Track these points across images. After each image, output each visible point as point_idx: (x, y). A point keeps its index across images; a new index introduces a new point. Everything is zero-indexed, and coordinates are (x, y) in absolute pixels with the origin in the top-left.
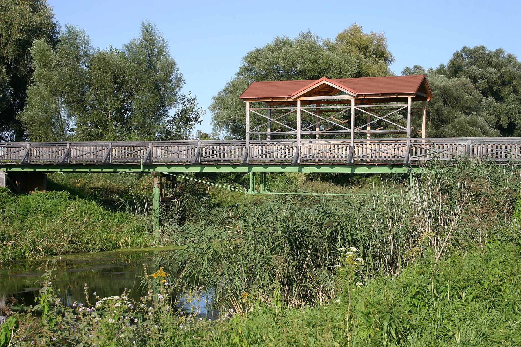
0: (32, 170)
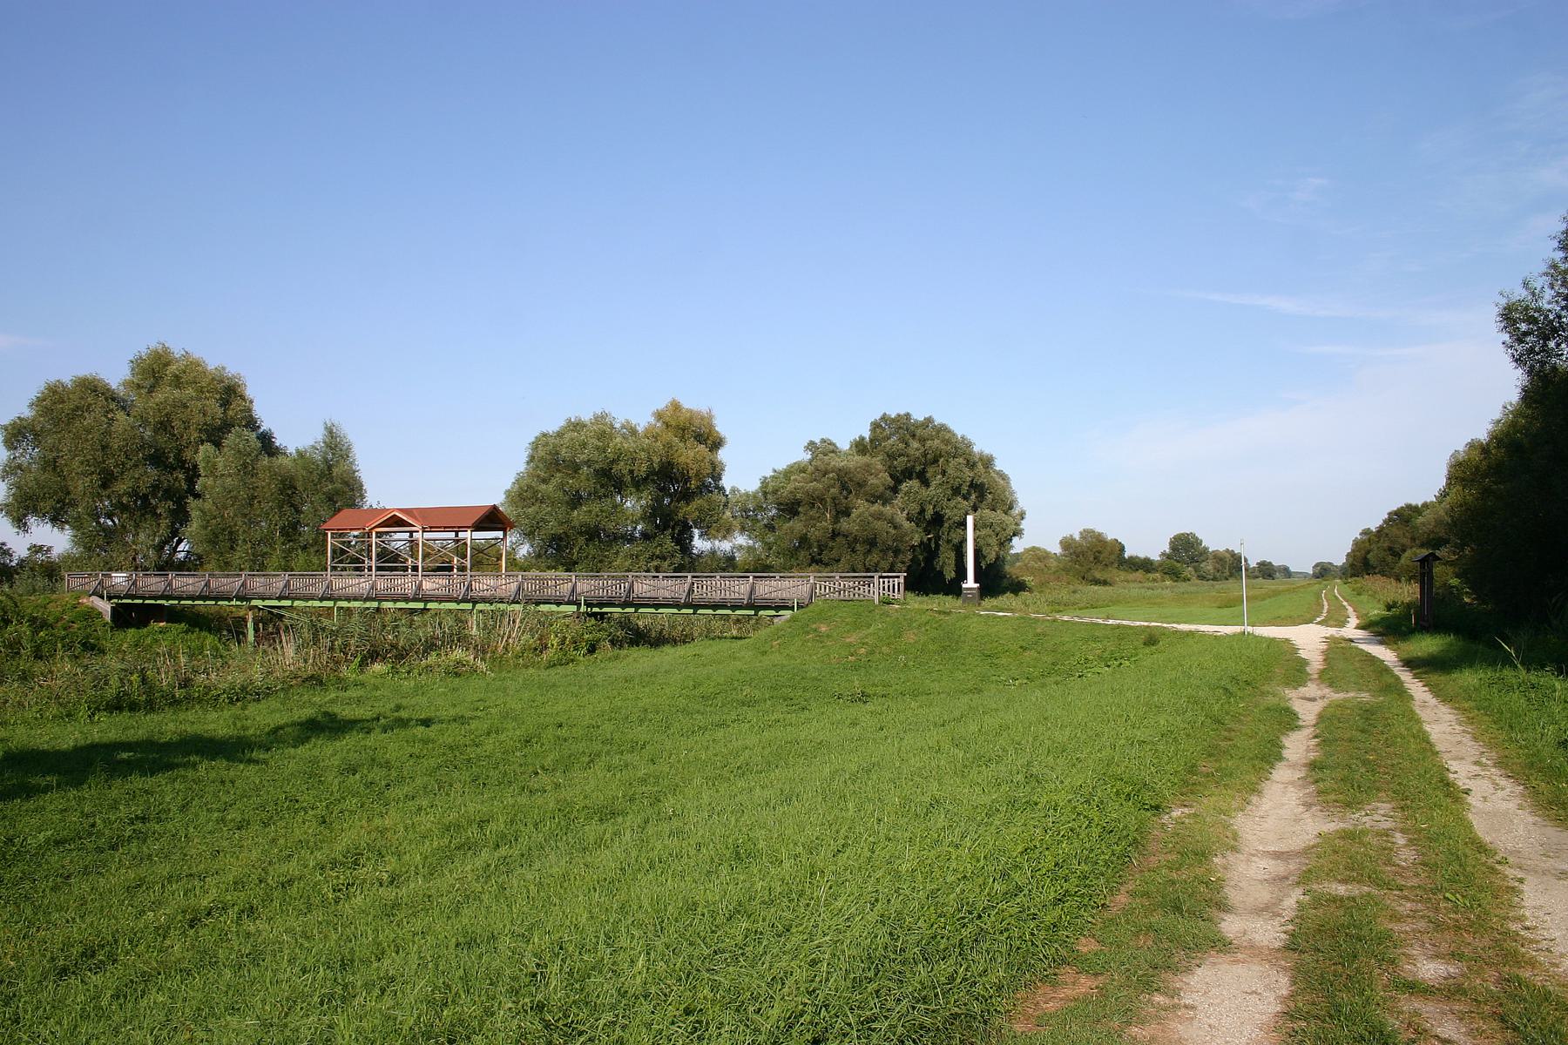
0: (141, 601)
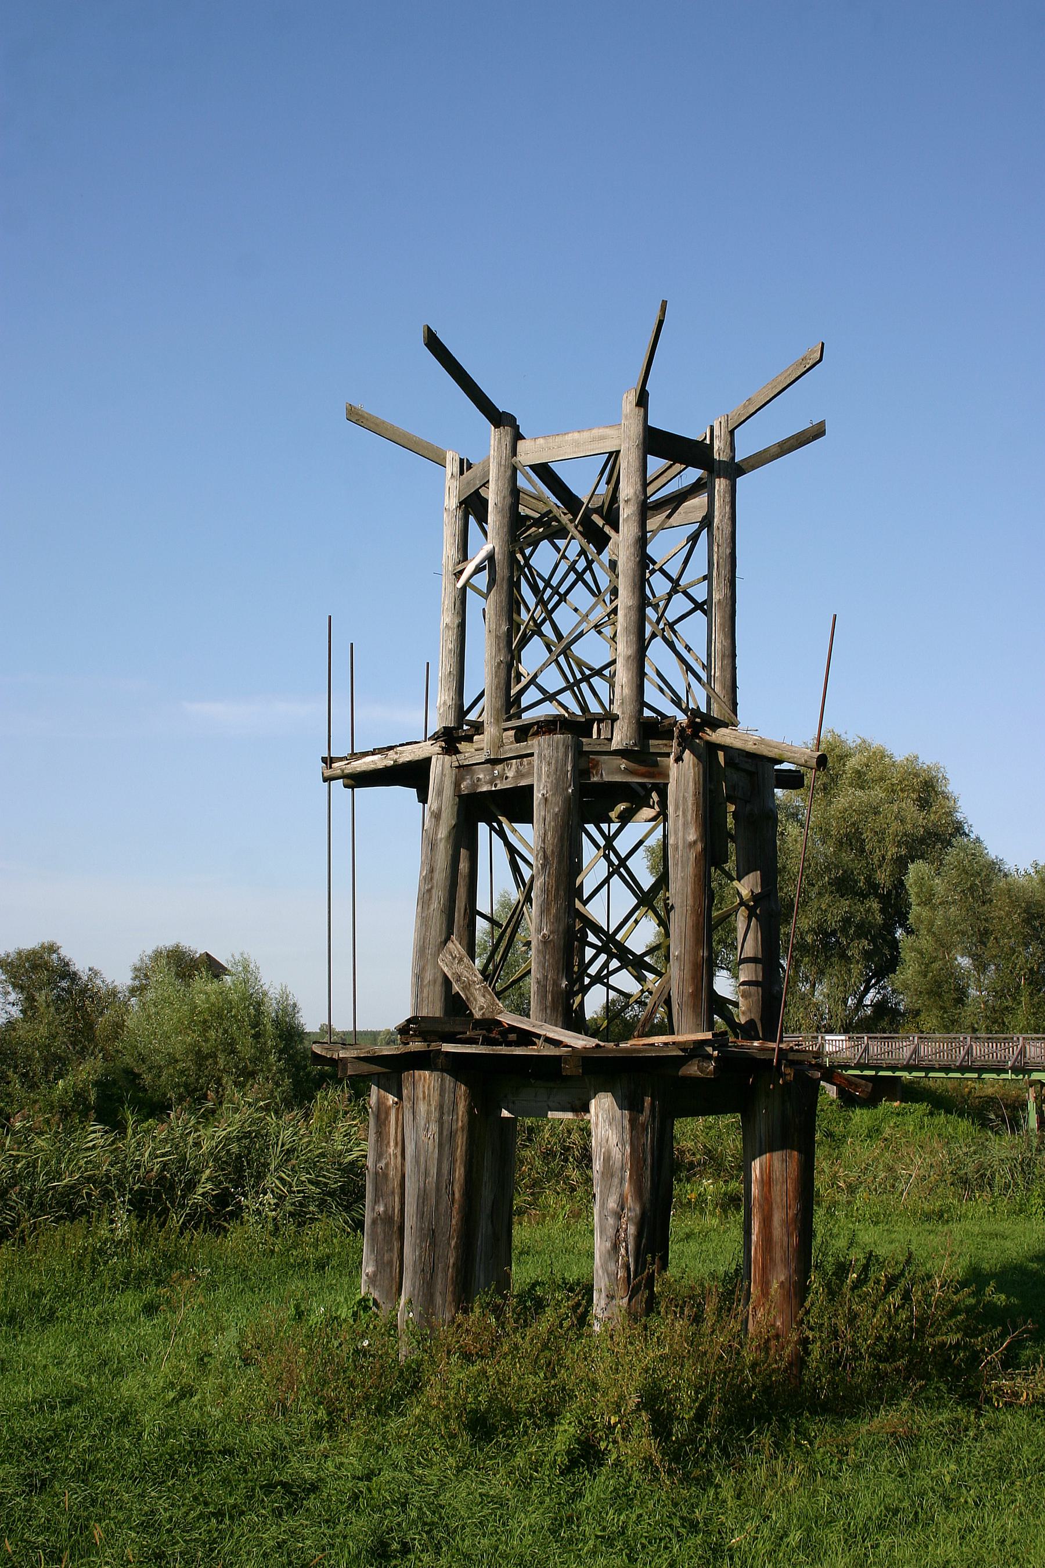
0: (873, 1073)
